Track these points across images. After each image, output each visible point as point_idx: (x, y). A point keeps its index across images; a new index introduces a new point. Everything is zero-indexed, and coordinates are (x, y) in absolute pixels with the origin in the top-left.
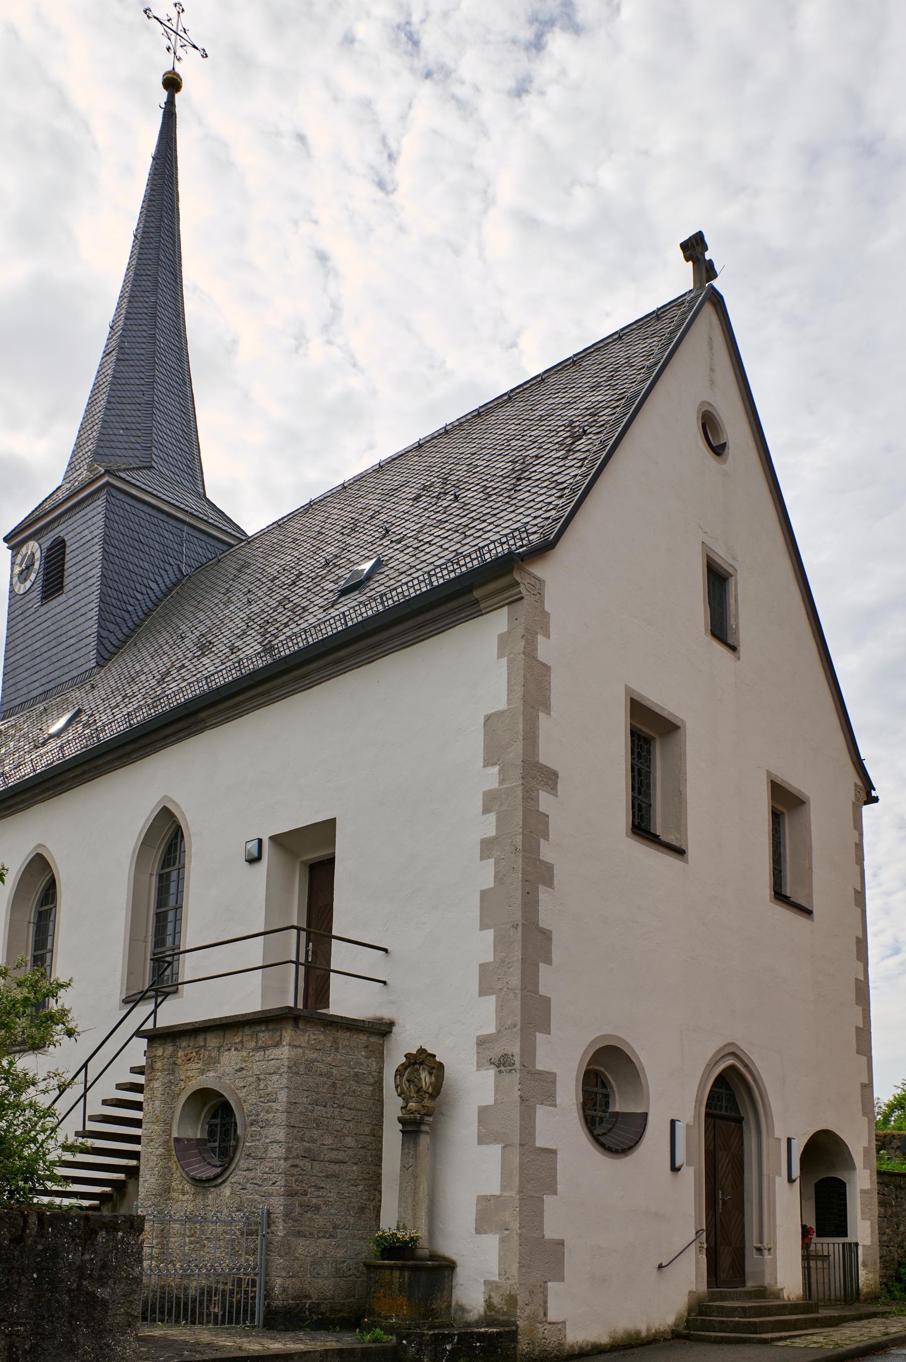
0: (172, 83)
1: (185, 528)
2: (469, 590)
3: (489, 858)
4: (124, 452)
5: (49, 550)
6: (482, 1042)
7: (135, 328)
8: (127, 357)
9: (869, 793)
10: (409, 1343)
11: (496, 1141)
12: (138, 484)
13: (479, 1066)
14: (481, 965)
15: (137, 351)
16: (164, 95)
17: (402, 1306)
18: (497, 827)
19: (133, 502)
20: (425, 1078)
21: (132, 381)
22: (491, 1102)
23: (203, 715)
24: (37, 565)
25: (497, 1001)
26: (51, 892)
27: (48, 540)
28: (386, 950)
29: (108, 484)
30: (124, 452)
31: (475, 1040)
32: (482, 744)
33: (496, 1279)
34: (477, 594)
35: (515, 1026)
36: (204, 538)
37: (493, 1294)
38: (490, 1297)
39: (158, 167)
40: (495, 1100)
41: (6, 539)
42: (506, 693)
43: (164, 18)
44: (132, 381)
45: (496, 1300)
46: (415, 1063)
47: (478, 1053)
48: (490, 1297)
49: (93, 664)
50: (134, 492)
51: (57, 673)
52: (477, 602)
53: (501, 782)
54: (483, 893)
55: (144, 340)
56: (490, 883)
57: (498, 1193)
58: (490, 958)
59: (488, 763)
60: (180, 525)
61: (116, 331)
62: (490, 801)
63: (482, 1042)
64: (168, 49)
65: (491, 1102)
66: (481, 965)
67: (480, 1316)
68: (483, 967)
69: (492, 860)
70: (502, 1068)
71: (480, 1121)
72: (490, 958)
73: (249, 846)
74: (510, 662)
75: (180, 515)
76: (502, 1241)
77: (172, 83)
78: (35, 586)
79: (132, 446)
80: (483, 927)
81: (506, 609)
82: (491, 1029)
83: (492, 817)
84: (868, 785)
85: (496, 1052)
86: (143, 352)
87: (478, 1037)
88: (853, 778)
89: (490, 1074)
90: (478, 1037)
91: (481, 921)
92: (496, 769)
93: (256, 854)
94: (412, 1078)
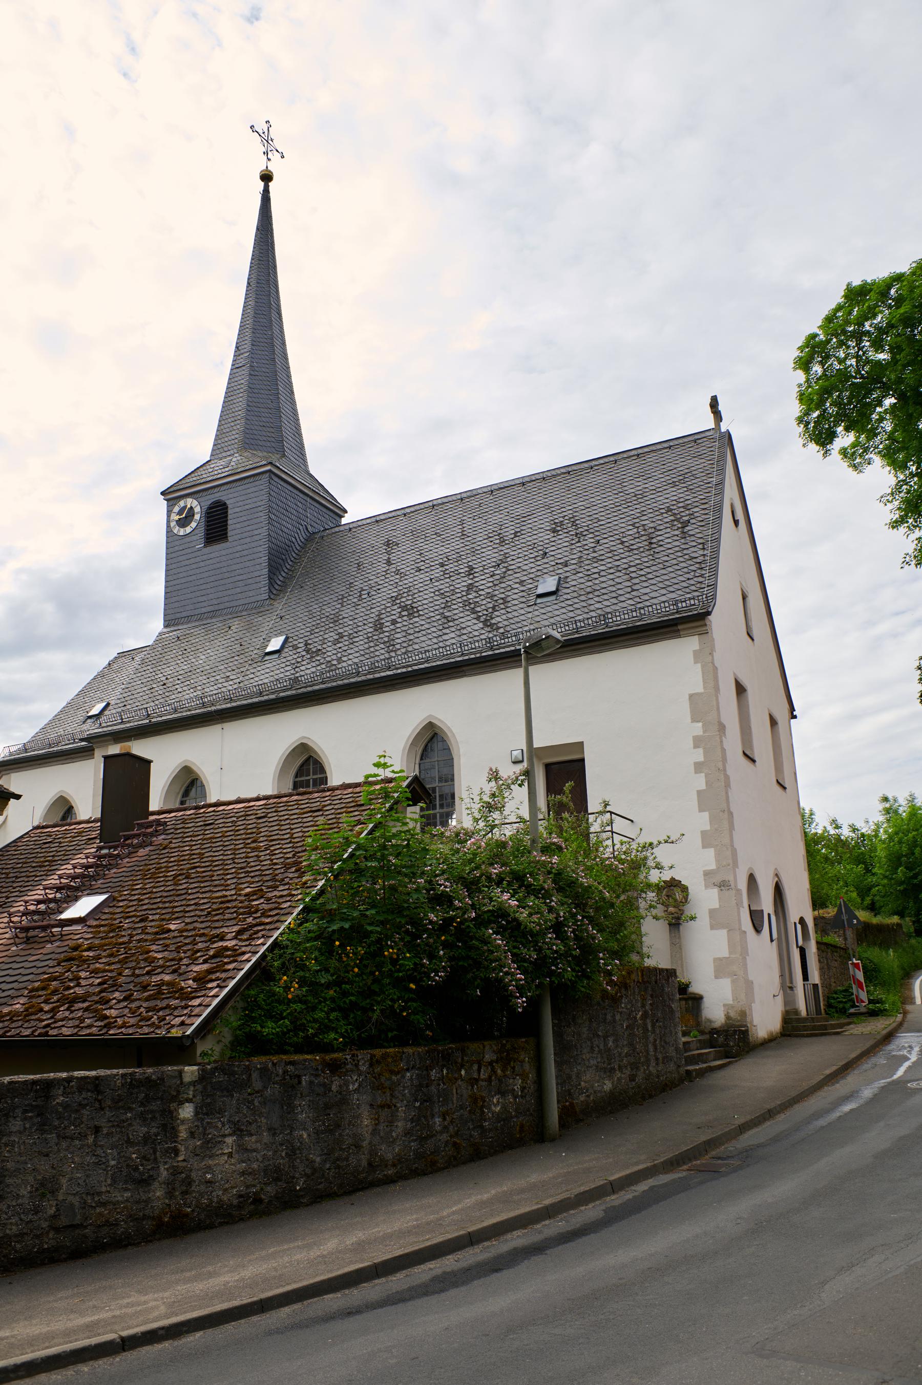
0: (267, 177)
1: (308, 499)
2: (676, 625)
3: (701, 772)
4: (264, 443)
5: (209, 508)
6: (707, 874)
7: (260, 352)
8: (256, 373)
9: (792, 713)
10: (719, 1036)
11: (723, 927)
12: (286, 471)
13: (707, 887)
14: (702, 832)
15: (264, 370)
16: (261, 185)
17: (689, 1020)
18: (705, 757)
19: (282, 483)
20: (678, 896)
21: (262, 391)
22: (717, 906)
23: (464, 668)
24: (197, 517)
25: (715, 851)
26: (305, 767)
27: (209, 499)
28: (632, 821)
29: (270, 471)
30: (264, 443)
31: (702, 873)
32: (689, 709)
33: (731, 1002)
34: (680, 627)
35: (729, 865)
36: (317, 505)
37: (730, 1011)
38: (728, 1013)
39: (262, 236)
40: (720, 906)
41: (163, 493)
42: (702, 683)
43: (261, 132)
44: (262, 391)
45: (732, 1014)
46: (671, 886)
47: (705, 880)
48: (728, 1013)
49: (265, 596)
50: (284, 476)
51: (226, 599)
52: (679, 630)
53: (704, 732)
54: (699, 792)
55: (267, 362)
56: (703, 786)
57: (727, 956)
58: (708, 828)
59: (694, 720)
60: (305, 498)
61: (242, 351)
62: (698, 742)
63: (707, 874)
64: (264, 153)
65: (717, 906)
66: (702, 832)
67: (722, 1024)
68: (703, 833)
69: (703, 775)
70: (722, 888)
71: (710, 917)
72: (708, 828)
73: (515, 753)
74: (703, 667)
75: (306, 491)
76: (733, 982)
77: (267, 177)
78: (196, 532)
79: (269, 439)
80: (701, 810)
81: (697, 636)
82: (713, 866)
83: (701, 751)
84: (792, 709)
85: (718, 879)
86: (267, 371)
87: (704, 871)
88: (787, 706)
89: (715, 891)
90: (704, 871)
91: (699, 807)
92: (700, 724)
93: (521, 759)
94: (669, 894)
